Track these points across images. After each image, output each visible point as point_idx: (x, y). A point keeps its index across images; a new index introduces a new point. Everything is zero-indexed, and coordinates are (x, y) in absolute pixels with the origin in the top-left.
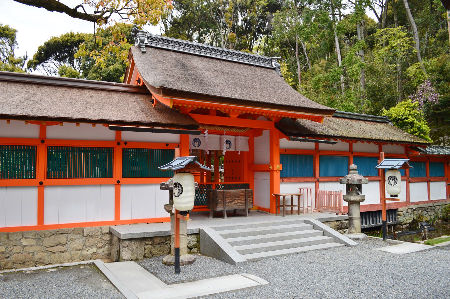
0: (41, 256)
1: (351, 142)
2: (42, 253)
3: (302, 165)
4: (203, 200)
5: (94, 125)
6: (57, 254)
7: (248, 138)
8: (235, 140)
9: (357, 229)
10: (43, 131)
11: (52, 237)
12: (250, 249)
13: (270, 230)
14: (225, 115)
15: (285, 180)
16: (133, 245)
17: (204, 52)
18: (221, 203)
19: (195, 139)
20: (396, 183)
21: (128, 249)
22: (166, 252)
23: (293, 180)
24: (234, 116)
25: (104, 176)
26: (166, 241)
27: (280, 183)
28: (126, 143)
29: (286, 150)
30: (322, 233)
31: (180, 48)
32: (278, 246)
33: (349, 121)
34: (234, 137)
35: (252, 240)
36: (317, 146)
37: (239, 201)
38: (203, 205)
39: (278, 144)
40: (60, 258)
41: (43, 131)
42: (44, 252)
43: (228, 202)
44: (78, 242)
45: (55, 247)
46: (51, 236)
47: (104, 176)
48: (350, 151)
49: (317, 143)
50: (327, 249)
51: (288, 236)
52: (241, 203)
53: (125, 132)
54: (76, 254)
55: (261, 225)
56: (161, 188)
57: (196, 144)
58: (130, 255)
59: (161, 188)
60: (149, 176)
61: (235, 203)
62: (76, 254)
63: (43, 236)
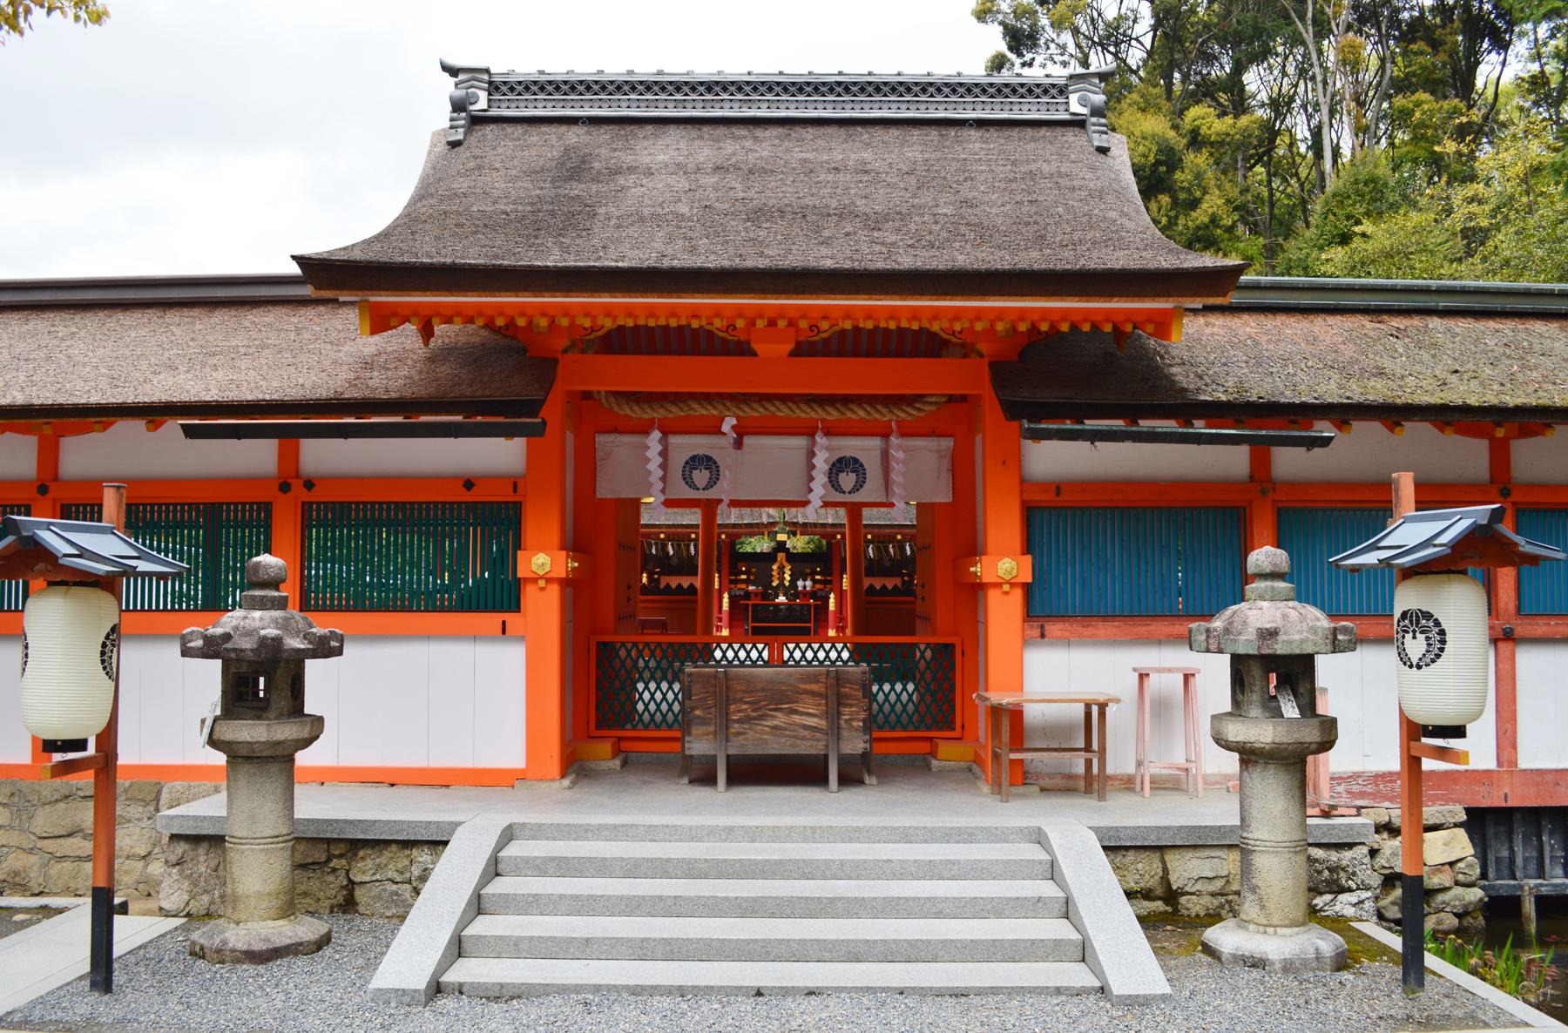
0: (18, 866)
1: (1500, 433)
2: (23, 856)
3: (1147, 558)
4: (904, 706)
5: (154, 426)
6: (67, 865)
7: (947, 443)
8: (885, 456)
9: (1271, 906)
10: (49, 455)
11: (62, 805)
12: (553, 939)
13: (780, 863)
14: (742, 349)
15: (1053, 628)
16: (202, 859)
17: (728, 105)
18: (704, 722)
19: (693, 458)
20: (1437, 650)
21: (181, 873)
22: (327, 903)
23: (1104, 628)
24: (773, 349)
25: (498, 606)
26: (329, 860)
27: (1026, 642)
28: (309, 484)
29: (1058, 487)
30: (1060, 907)
31: (625, 104)
32: (708, 943)
33: (1507, 327)
34: (875, 442)
35: (621, 898)
36: (1260, 460)
37: (796, 718)
38: (904, 729)
39: (1014, 460)
40: (75, 878)
41: (49, 455)
42: (31, 851)
43: (740, 721)
44: (137, 830)
45: (62, 841)
46: (57, 801)
47: (498, 606)
48: (1492, 481)
49: (1261, 450)
50: (959, 994)
51: (832, 900)
52: (806, 727)
53: (1047, 445)
54: (127, 872)
55: (787, 834)
56: (186, 653)
57: (701, 477)
58: (186, 897)
59: (186, 653)
60: (490, 606)
61: (776, 727)
62: (127, 872)
63: (34, 798)
